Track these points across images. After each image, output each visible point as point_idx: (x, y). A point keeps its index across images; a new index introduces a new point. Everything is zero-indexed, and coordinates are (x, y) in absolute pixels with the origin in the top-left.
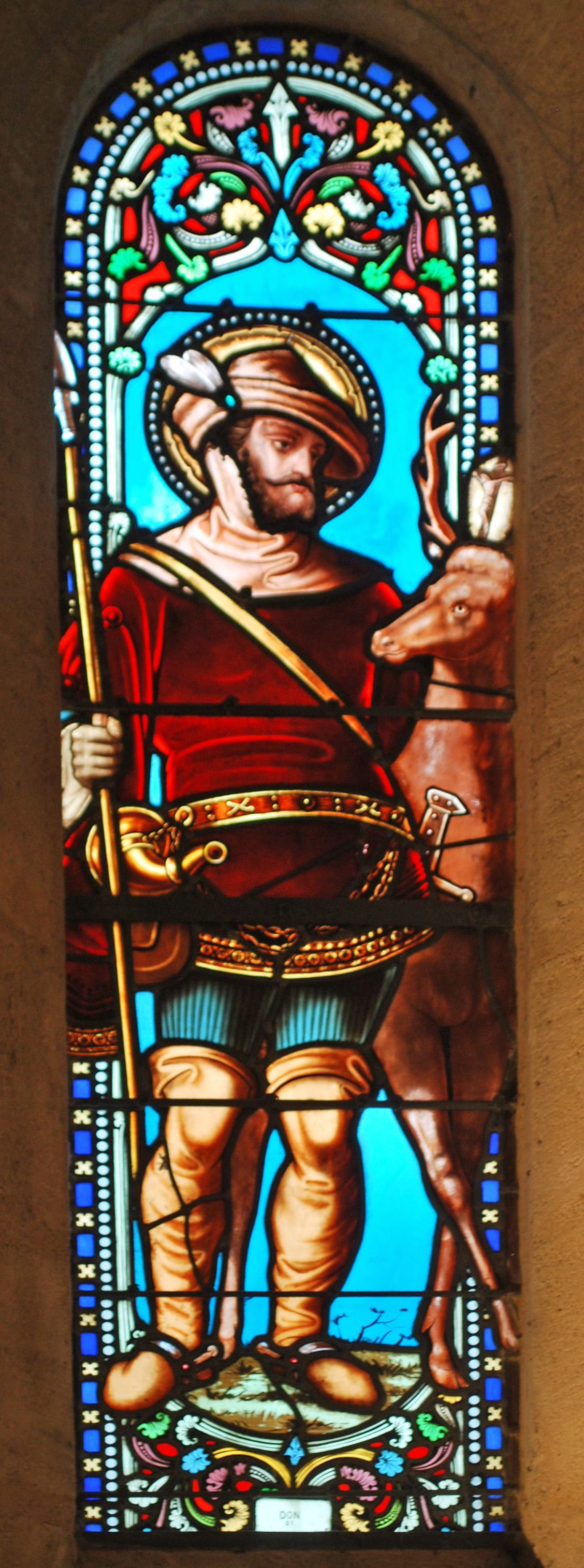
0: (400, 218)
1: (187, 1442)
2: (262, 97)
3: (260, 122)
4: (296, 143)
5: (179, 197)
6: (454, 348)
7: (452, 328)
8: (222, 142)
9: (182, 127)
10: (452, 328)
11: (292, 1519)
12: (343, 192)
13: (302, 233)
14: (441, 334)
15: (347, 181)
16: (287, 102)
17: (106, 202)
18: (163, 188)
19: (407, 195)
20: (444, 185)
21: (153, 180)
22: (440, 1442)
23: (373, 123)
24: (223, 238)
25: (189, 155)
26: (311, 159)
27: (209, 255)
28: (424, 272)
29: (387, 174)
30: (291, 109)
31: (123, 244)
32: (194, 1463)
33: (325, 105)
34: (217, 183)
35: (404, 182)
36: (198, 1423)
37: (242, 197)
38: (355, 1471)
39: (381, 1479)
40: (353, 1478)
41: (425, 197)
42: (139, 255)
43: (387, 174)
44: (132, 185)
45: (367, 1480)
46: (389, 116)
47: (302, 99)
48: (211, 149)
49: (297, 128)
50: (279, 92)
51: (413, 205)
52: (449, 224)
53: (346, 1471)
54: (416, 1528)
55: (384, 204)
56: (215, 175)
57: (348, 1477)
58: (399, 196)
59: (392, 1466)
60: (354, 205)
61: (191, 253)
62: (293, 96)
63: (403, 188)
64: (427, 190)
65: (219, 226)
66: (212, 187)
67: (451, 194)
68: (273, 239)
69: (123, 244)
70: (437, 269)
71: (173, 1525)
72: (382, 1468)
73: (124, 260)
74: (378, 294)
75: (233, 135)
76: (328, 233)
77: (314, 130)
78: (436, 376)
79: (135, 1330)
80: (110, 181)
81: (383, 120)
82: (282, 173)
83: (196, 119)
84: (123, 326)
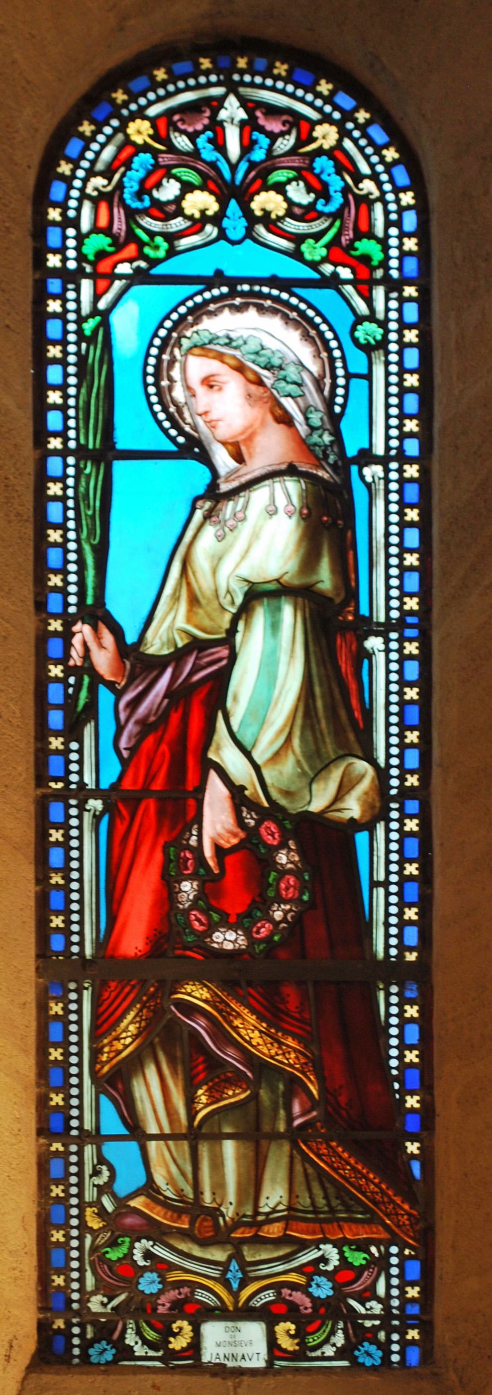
0: (338, 200)
1: (141, 1263)
2: (217, 104)
3: (217, 128)
4: (246, 142)
5: (143, 191)
6: (380, 315)
7: (379, 293)
8: (182, 142)
9: (151, 132)
10: (379, 293)
11: (235, 1333)
12: (289, 181)
13: (251, 219)
14: (369, 301)
15: (292, 174)
16: (238, 108)
17: (83, 196)
18: (133, 180)
19: (342, 184)
20: (375, 177)
21: (123, 175)
22: (362, 1269)
23: (313, 124)
24: (182, 223)
25: (155, 153)
26: (258, 155)
27: (172, 238)
28: (356, 249)
29: (323, 164)
30: (242, 115)
31: (96, 229)
32: (149, 1284)
33: (272, 111)
34: (178, 179)
35: (338, 172)
36: (152, 1246)
37: (202, 188)
38: (294, 1293)
39: (314, 1300)
40: (291, 1298)
41: (357, 186)
42: (109, 240)
43: (323, 164)
44: (105, 182)
45: (298, 1297)
46: (327, 119)
47: (250, 105)
48: (172, 149)
49: (247, 129)
50: (232, 102)
51: (346, 191)
52: (378, 208)
53: (286, 1292)
54: (343, 1345)
55: (323, 192)
56: (174, 171)
57: (287, 1298)
58: (335, 183)
59: (323, 1289)
60: (299, 194)
61: (152, 234)
62: (244, 103)
63: (338, 178)
64: (358, 178)
65: (179, 212)
66: (172, 181)
67: (379, 184)
68: (226, 223)
69: (96, 229)
70: (366, 246)
71: (127, 1342)
72: (314, 1290)
73: (96, 243)
74: (314, 265)
75: (193, 137)
76: (273, 216)
77: (262, 130)
78: (366, 339)
79: (98, 1164)
80: (85, 181)
81: (320, 122)
82: (234, 168)
83: (162, 125)
84: (97, 297)
